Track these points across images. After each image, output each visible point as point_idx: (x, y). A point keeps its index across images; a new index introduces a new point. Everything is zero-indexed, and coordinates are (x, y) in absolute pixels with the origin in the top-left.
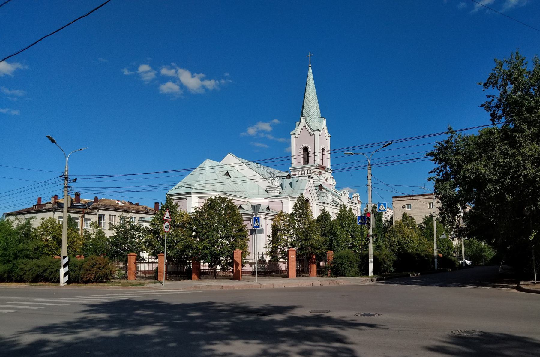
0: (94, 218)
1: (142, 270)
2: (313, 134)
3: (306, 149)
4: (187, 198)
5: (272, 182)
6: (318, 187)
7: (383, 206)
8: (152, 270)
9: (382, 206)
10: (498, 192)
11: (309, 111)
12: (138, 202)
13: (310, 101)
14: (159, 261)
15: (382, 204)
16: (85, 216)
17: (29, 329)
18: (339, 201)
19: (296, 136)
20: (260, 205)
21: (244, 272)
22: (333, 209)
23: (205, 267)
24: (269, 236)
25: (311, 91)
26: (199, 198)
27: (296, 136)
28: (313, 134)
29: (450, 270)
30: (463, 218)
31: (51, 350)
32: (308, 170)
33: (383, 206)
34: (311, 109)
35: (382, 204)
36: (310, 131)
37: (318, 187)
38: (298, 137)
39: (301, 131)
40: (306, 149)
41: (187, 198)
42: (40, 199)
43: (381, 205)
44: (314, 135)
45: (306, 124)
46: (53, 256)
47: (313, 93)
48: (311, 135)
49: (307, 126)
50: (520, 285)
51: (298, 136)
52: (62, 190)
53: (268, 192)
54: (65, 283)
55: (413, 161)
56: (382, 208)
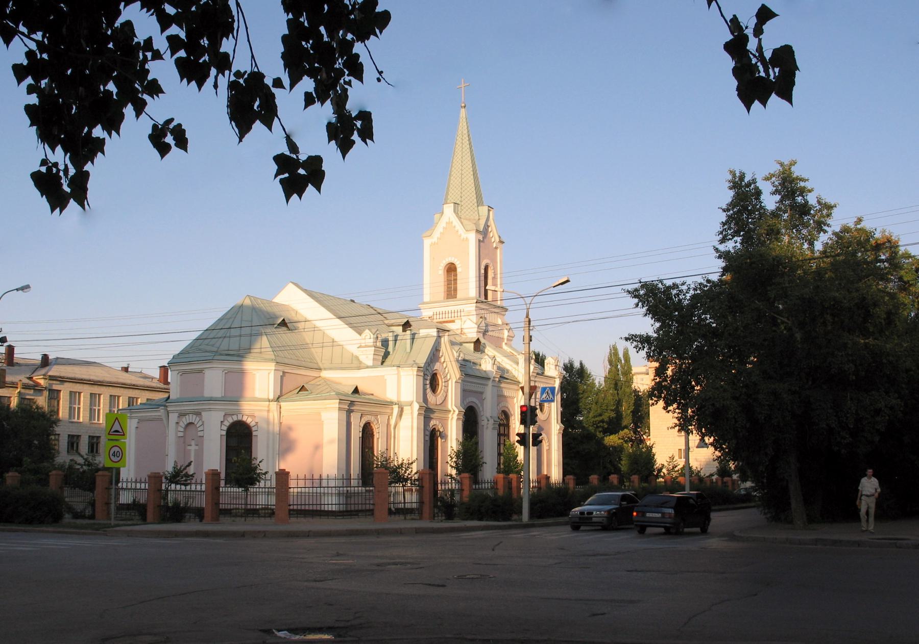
1: (123, 503)
6: (473, 344)
7: (549, 392)
8: (125, 503)
9: (548, 392)
10: (678, 386)
12: (126, 366)
14: (148, 487)
15: (548, 389)
21: (293, 510)
22: (211, 540)
23: (229, 490)
24: (860, 220)
29: (342, 136)
31: (372, 449)
33: (549, 392)
35: (548, 389)
43: (547, 391)
54: (581, 364)
56: (548, 397)
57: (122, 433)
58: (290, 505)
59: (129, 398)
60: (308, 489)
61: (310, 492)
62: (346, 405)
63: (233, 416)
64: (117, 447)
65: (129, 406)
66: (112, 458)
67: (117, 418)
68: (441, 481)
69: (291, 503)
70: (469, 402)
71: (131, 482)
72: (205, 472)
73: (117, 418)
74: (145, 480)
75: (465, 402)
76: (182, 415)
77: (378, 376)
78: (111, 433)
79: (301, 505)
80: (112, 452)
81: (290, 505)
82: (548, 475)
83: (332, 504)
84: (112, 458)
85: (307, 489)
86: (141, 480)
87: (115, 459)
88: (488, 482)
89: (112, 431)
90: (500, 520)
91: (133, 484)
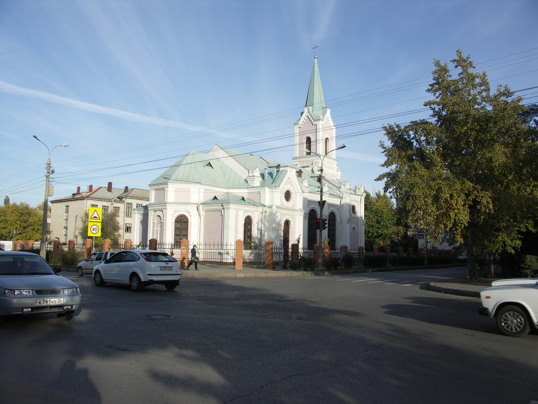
0: (123, 207)
2: (315, 124)
3: (309, 140)
4: (165, 188)
5: (252, 173)
6: (317, 178)
11: (312, 101)
13: (314, 87)
16: (320, 199)
17: (199, 219)
18: (339, 193)
19: (299, 127)
20: (325, 201)
25: (315, 81)
26: (175, 189)
27: (299, 127)
28: (315, 124)
30: (518, 218)
32: (304, 162)
34: (315, 99)
36: (312, 121)
37: (317, 178)
38: (300, 127)
39: (304, 121)
40: (309, 140)
41: (165, 188)
42: (79, 188)
44: (316, 125)
45: (309, 115)
46: (510, 158)
47: (318, 84)
48: (313, 125)
49: (310, 117)
50: (304, 211)
51: (301, 126)
52: (54, 173)
53: (248, 182)
55: (199, 222)
57: (99, 218)
58: (189, 259)
59: (137, 204)
60: (207, 250)
61: (206, 251)
62: (220, 206)
63: (179, 212)
64: (96, 226)
65: (137, 207)
66: (93, 231)
67: (96, 210)
68: (303, 248)
69: (189, 258)
70: (331, 210)
71: (279, 249)
72: (149, 240)
73: (96, 210)
74: (144, 245)
75: (309, 207)
76: (155, 211)
77: (365, 205)
78: (92, 218)
79: (207, 259)
80: (92, 228)
81: (189, 259)
82: (157, 240)
83: (218, 259)
84: (93, 231)
85: (211, 250)
86: (144, 245)
87: (95, 232)
88: (277, 248)
89: (93, 216)
90: (309, 269)
91: (278, 250)
